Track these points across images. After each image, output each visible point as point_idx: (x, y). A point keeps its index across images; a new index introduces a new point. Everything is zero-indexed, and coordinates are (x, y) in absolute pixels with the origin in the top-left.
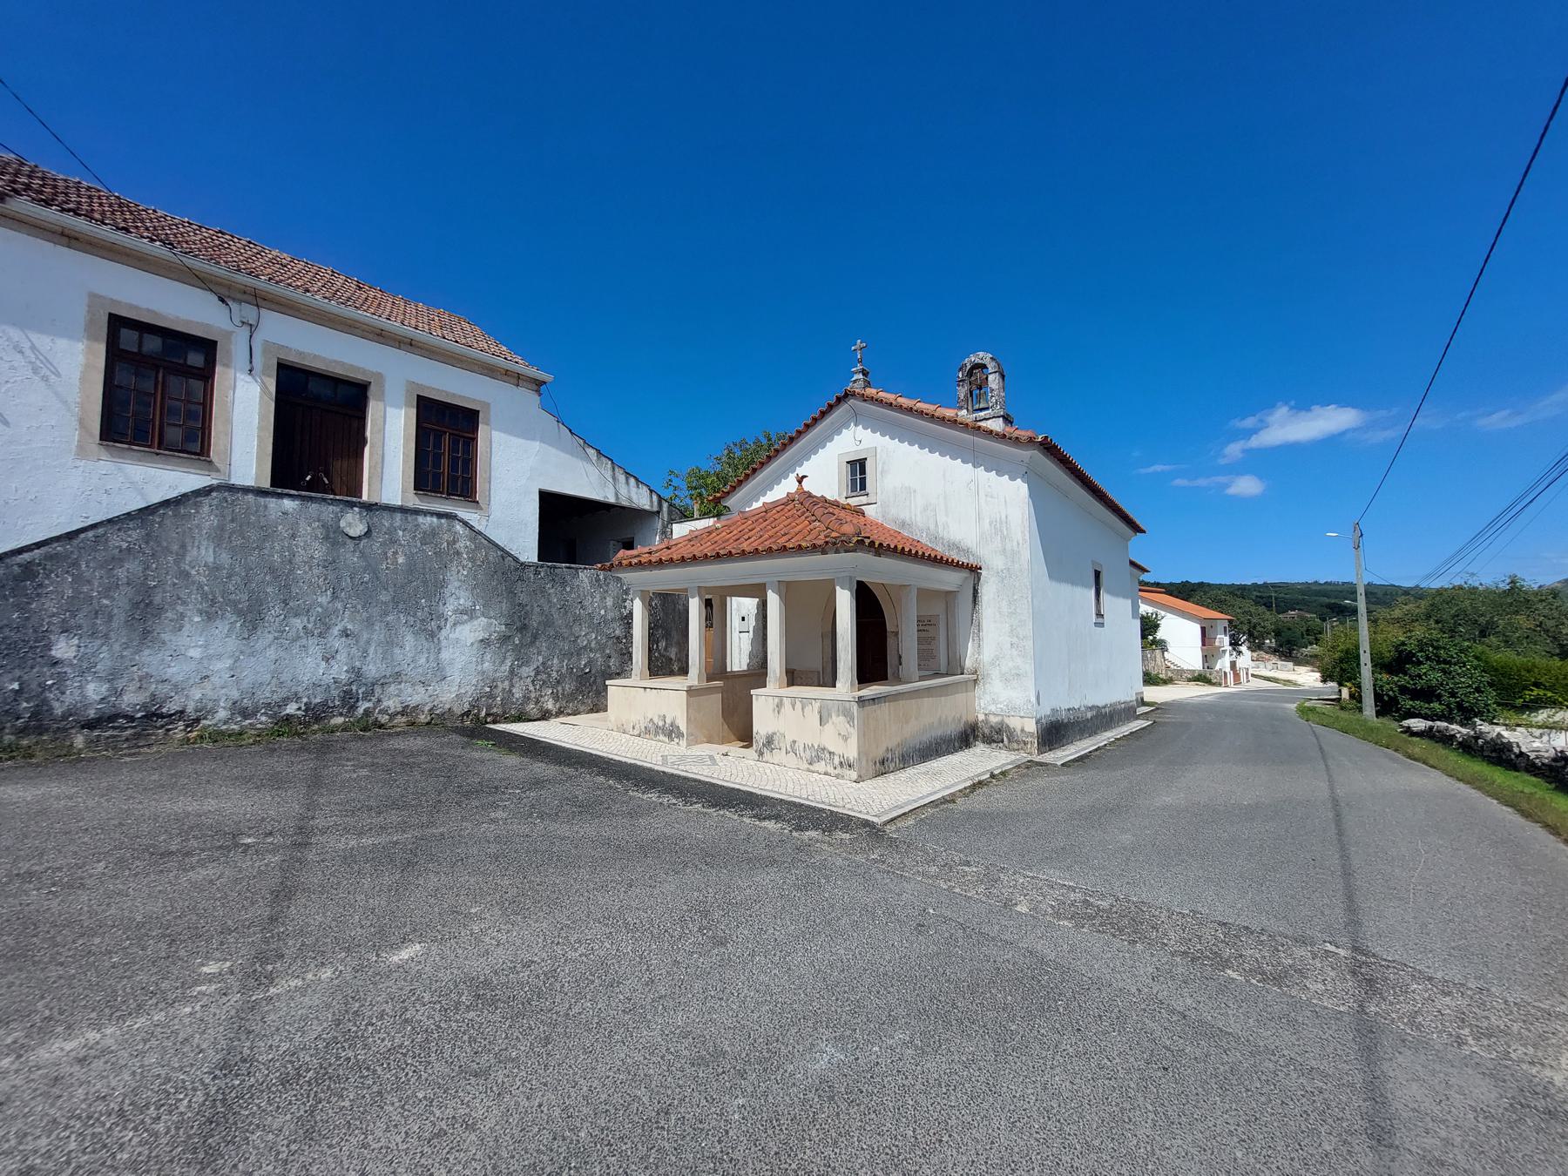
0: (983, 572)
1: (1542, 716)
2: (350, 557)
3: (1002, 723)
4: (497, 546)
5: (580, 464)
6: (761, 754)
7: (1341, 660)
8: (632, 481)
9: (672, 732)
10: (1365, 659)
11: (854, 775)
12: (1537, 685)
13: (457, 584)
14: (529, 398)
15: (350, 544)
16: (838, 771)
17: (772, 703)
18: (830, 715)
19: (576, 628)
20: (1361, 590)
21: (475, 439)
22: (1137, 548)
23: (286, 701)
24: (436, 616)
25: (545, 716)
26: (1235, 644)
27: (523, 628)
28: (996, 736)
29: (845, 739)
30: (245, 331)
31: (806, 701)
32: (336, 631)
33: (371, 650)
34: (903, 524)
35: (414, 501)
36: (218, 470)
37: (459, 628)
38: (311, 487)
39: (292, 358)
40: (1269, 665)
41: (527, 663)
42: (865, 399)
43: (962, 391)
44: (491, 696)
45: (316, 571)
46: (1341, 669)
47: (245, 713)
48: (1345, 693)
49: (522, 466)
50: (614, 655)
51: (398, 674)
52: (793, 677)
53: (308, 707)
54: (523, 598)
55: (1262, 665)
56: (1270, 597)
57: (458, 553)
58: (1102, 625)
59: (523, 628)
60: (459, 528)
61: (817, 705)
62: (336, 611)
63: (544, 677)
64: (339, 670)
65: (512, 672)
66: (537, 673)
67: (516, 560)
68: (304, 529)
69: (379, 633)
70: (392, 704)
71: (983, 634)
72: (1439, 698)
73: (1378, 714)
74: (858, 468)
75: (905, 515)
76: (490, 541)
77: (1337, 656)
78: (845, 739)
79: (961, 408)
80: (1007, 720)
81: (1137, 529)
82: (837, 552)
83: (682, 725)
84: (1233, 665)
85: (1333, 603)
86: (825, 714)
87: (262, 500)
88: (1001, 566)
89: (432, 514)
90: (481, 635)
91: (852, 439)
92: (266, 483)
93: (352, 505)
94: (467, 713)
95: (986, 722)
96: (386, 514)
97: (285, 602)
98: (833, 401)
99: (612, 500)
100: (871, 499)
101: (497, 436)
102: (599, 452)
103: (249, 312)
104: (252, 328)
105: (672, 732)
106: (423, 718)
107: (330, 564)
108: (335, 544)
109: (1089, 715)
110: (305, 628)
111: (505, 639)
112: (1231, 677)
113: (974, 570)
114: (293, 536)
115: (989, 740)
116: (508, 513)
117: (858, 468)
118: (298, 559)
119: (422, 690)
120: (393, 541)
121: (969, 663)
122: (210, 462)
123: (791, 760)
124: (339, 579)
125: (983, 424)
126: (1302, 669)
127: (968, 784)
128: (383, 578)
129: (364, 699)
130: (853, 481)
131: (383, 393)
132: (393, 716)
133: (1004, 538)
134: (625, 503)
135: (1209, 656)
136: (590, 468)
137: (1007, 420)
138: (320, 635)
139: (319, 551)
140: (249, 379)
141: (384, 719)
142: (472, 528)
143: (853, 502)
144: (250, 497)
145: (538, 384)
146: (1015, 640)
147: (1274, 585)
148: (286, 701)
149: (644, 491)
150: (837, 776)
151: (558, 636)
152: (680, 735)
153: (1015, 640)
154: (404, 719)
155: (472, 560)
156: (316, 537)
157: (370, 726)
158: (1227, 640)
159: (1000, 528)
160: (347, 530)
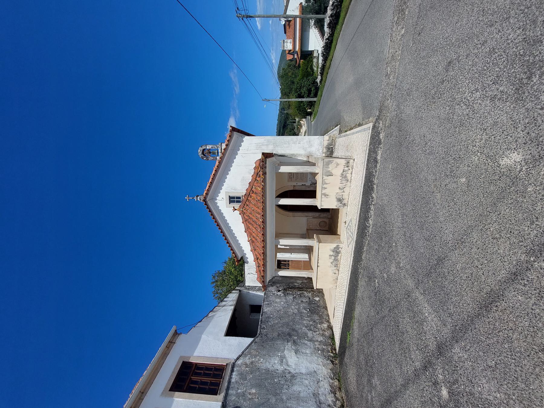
1: (315, 69)
3: (326, 147)
4: (250, 345)
5: (215, 319)
6: (345, 204)
9: (337, 252)
12: (307, 69)
13: (267, 363)
14: (182, 339)
16: (350, 168)
17: (324, 199)
18: (329, 171)
19: (290, 313)
20: (281, 100)
21: (196, 364)
24: (283, 375)
25: (330, 328)
27: (290, 335)
29: (338, 164)
31: (324, 183)
37: (290, 363)
41: (306, 334)
44: (323, 350)
49: (213, 343)
50: (301, 299)
51: (314, 394)
52: (312, 194)
54: (275, 334)
57: (252, 363)
59: (290, 335)
60: (239, 362)
61: (325, 177)
63: (312, 327)
65: (310, 341)
66: (311, 330)
72: (310, 88)
78: (338, 164)
79: (216, 159)
80: (325, 146)
82: (266, 167)
83: (334, 245)
86: (328, 174)
88: (272, 146)
89: (231, 374)
90: (293, 353)
94: (332, 362)
96: (229, 398)
99: (233, 307)
101: (196, 354)
102: (211, 311)
105: (337, 252)
106: (336, 383)
111: (295, 342)
117: (232, 200)
120: (244, 395)
123: (347, 190)
126: (301, 131)
128: (263, 401)
132: (337, 399)
133: (263, 145)
134: (235, 302)
136: (217, 316)
142: (240, 356)
146: (298, 142)
149: (230, 295)
150: (352, 168)
152: (337, 247)
153: (298, 142)
154: (338, 393)
155: (255, 356)
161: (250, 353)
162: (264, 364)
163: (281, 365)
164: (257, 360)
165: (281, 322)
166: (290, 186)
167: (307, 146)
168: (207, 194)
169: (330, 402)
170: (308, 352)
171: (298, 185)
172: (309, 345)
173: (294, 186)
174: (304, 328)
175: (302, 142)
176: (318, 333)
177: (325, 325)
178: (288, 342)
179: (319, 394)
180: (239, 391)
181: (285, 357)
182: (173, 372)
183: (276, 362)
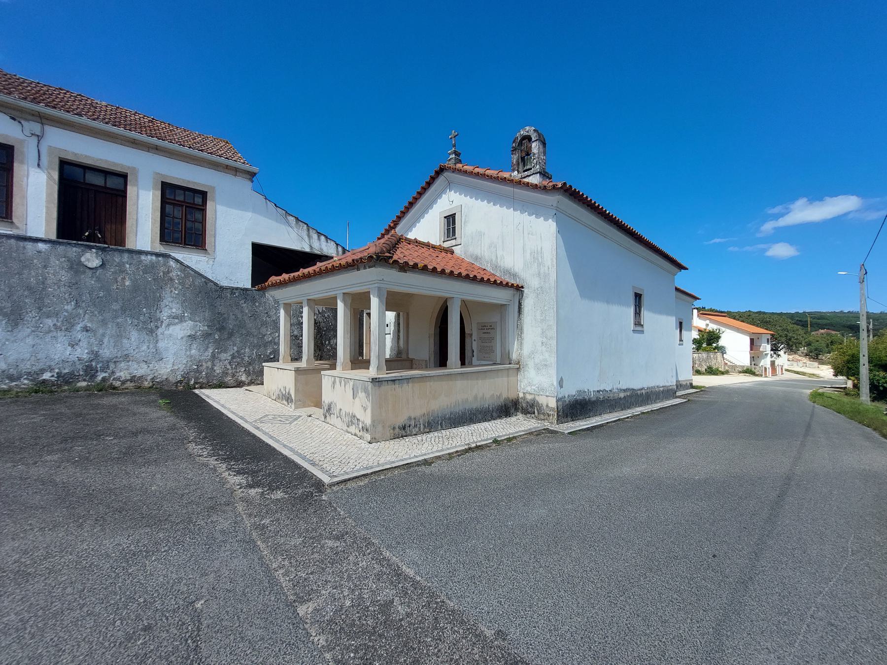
0: (526, 290)
2: (89, 281)
3: (534, 400)
4: (201, 275)
7: (848, 362)
8: (323, 238)
10: (864, 360)
11: (368, 437)
14: (242, 185)
15: (89, 273)
17: (331, 379)
22: (682, 280)
23: (43, 371)
26: (775, 349)
27: (221, 329)
28: (530, 409)
29: (365, 409)
30: (34, 140)
32: (78, 327)
33: (106, 340)
34: (477, 258)
35: (160, 248)
36: (17, 228)
37: (171, 328)
38: (88, 239)
39: (70, 157)
40: (801, 364)
41: (225, 351)
42: (455, 170)
43: (515, 158)
44: (198, 371)
45: (62, 289)
46: (847, 367)
47: (11, 378)
48: (850, 384)
49: (238, 228)
51: (127, 356)
53: (59, 375)
54: (222, 309)
55: (795, 364)
56: (802, 321)
57: (171, 279)
58: (642, 332)
60: (172, 263)
61: (351, 383)
62: (78, 315)
64: (82, 352)
65: (213, 356)
67: (216, 284)
68: (54, 262)
69: (111, 329)
70: (123, 374)
71: (525, 335)
73: (874, 399)
74: (451, 220)
75: (477, 252)
76: (196, 272)
77: (847, 357)
79: (513, 171)
80: (537, 398)
81: (681, 267)
84: (773, 363)
85: (848, 325)
87: (21, 244)
91: (449, 200)
92: (53, 236)
93: (123, 251)
94: (180, 382)
95: (524, 398)
97: (40, 309)
98: (433, 174)
99: (307, 249)
100: (458, 241)
101: (220, 209)
102: (297, 219)
103: (36, 127)
104: (40, 138)
106: (146, 384)
107: (73, 285)
108: (77, 272)
109: (622, 395)
110: (55, 325)
111: (207, 336)
112: (769, 371)
113: (519, 289)
114: (45, 267)
115: (526, 412)
116: (227, 258)
117: (451, 220)
118: (49, 282)
119: (145, 366)
120: (122, 271)
121: (514, 356)
122: (12, 222)
124: (80, 295)
125: (526, 180)
127: (466, 447)
129: (102, 371)
130: (448, 230)
131: (137, 180)
132: (124, 382)
133: (539, 265)
135: (755, 356)
137: (544, 174)
138: (67, 330)
139: (65, 276)
140: (38, 170)
141: (117, 384)
142: (181, 263)
143: (446, 245)
144: (13, 241)
145: (252, 175)
146: (545, 340)
147: (810, 313)
148: (43, 371)
149: (332, 245)
151: (249, 334)
155: (182, 284)
156: (63, 268)
157: (107, 388)
158: (769, 347)
159: (537, 257)
160: (86, 263)
161: (187, 276)
162: (169, 295)
163: (169, 317)
164: (176, 286)
165: (245, 318)
166: (472, 329)
167: (537, 361)
168: (460, 171)
169: (118, 374)
170: (193, 351)
171: (474, 344)
172: (206, 354)
173: (471, 335)
174: (235, 348)
175: (544, 348)
176: (229, 367)
177: (243, 378)
178: (208, 326)
179: (128, 361)
180: (128, 266)
181: (181, 321)
182: (189, 182)
183: (174, 310)
